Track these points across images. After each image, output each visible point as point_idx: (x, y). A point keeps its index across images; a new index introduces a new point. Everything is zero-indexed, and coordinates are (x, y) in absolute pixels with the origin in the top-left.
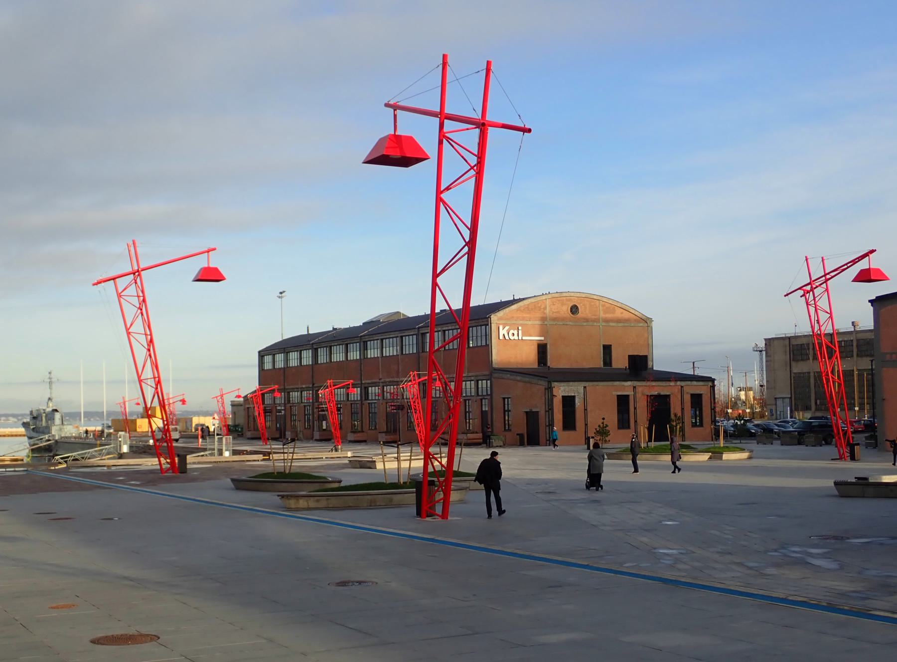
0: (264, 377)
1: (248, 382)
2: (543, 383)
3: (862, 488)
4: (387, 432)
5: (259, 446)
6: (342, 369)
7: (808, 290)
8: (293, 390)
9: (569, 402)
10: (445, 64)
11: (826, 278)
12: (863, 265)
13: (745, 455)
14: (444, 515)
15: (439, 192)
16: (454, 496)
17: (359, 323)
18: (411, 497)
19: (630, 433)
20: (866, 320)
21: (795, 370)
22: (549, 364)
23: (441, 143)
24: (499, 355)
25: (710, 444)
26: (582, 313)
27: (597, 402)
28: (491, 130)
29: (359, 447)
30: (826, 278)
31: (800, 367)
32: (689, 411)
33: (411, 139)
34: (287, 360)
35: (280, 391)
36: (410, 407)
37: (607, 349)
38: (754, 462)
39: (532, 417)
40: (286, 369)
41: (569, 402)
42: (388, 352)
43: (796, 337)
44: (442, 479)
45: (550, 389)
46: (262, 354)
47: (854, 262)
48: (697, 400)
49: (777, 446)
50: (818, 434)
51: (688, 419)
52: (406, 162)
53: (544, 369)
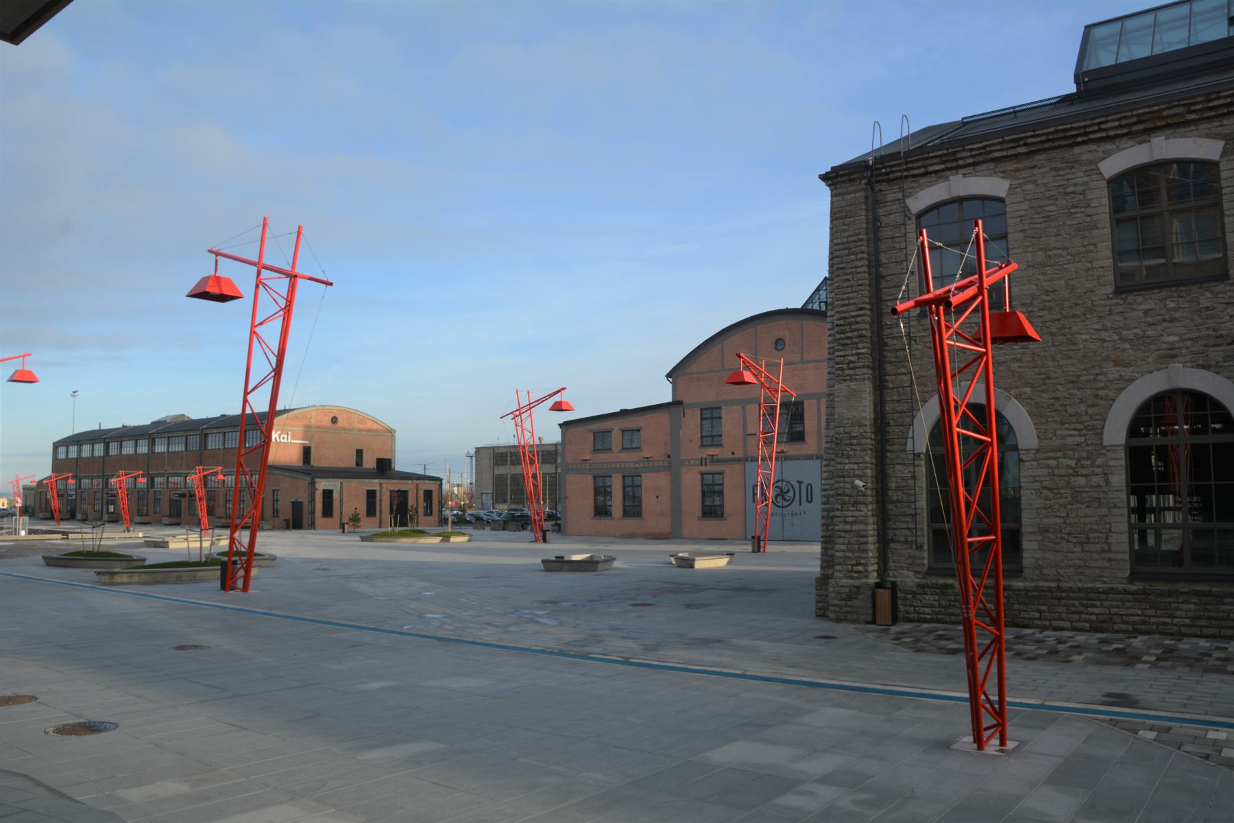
0: (58, 465)
1: (42, 469)
2: (309, 479)
3: (558, 564)
4: (170, 516)
5: (51, 525)
6: (131, 462)
7: (517, 414)
8: (85, 477)
9: (328, 494)
10: (265, 225)
11: (531, 406)
12: (557, 398)
13: (466, 538)
14: (245, 588)
15: (253, 326)
16: (254, 572)
17: (147, 422)
18: (216, 572)
19: (376, 519)
20: (553, 436)
21: (497, 472)
22: (312, 463)
23: (257, 286)
24: (275, 456)
25: (441, 530)
26: (340, 424)
27: (350, 495)
28: (301, 283)
29: (147, 528)
30: (531, 406)
31: (501, 470)
32: (422, 504)
33: (229, 281)
34: (80, 451)
35: (73, 477)
36: (192, 496)
37: (359, 453)
38: (473, 544)
39: (297, 506)
40: (78, 460)
41: (328, 494)
42: (173, 448)
43: (498, 447)
44: (244, 558)
45: (313, 483)
46: (56, 446)
47: (551, 396)
48: (428, 495)
49: (487, 531)
50: (518, 522)
51: (421, 510)
52: (223, 298)
53: (307, 466)
